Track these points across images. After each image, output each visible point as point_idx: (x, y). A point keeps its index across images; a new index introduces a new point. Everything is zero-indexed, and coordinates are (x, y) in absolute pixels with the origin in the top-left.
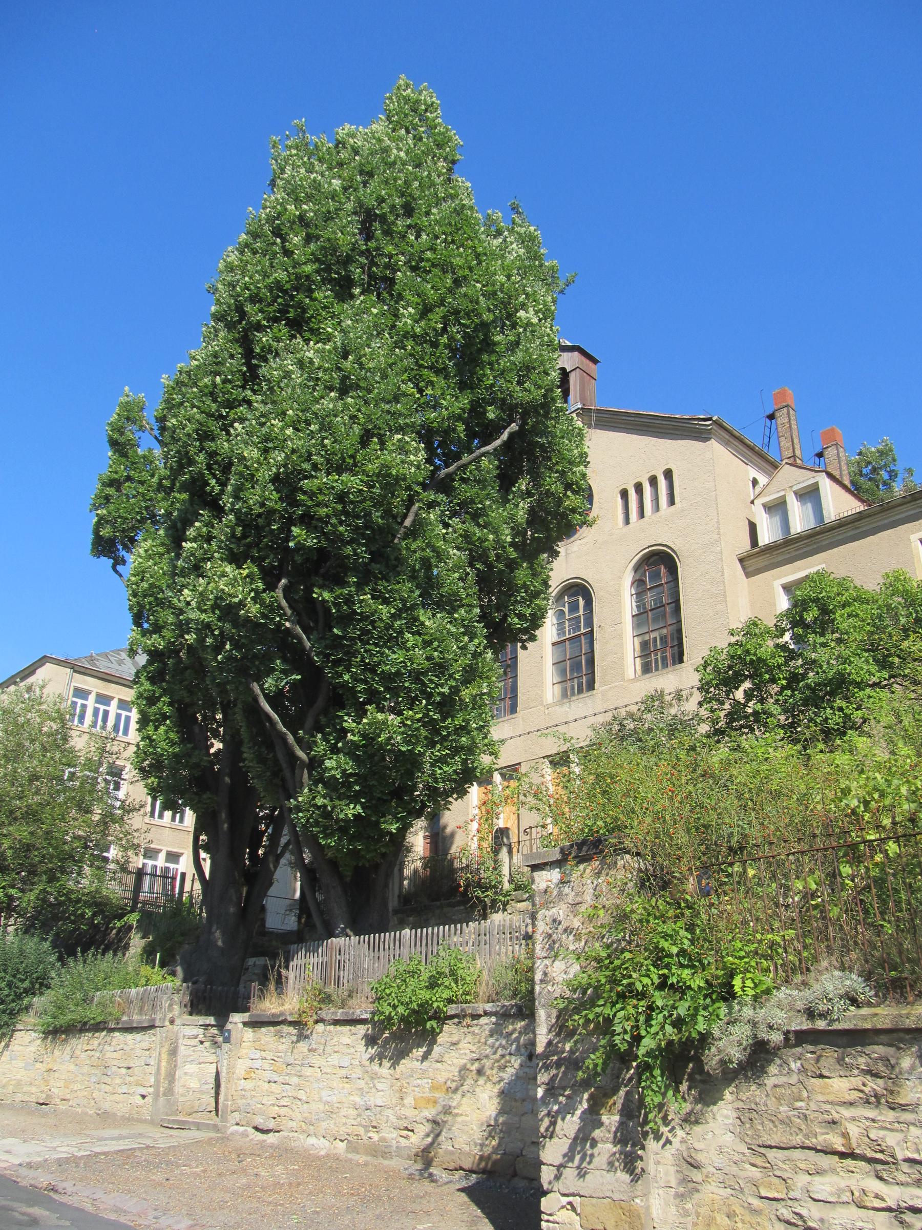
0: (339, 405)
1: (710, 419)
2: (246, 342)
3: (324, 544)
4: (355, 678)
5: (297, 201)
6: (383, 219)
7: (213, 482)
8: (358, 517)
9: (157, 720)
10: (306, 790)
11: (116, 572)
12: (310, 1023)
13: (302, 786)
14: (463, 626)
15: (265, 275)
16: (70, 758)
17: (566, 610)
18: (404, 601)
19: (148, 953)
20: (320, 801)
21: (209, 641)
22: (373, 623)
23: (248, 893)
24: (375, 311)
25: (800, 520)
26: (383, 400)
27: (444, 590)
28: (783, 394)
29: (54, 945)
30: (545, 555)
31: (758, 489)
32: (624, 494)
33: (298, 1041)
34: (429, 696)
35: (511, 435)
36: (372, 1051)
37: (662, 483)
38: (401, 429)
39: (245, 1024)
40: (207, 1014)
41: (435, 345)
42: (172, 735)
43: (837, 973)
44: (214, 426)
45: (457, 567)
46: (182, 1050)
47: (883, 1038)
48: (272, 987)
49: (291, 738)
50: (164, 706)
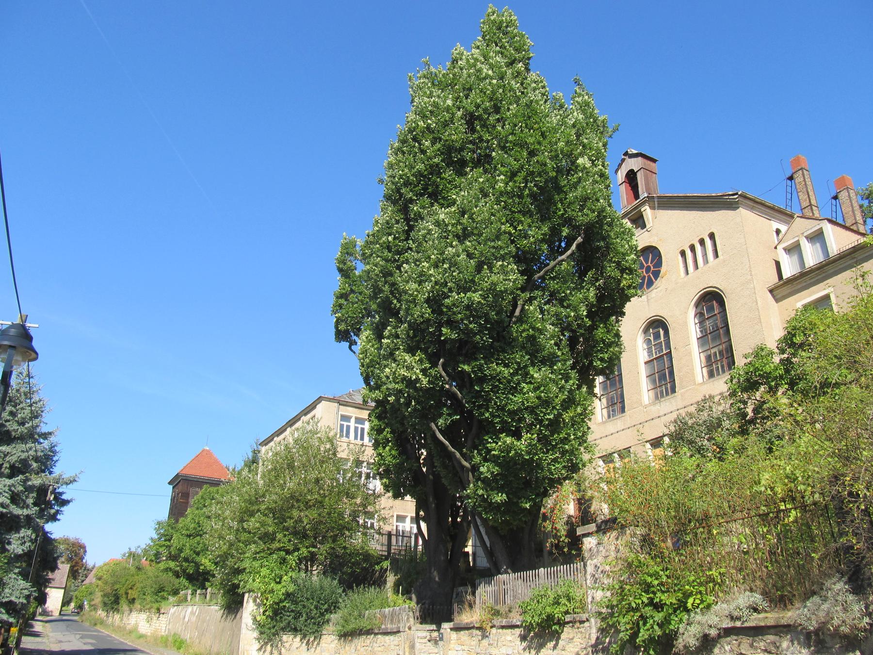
0: (463, 251)
1: (736, 194)
2: (405, 210)
3: (462, 336)
4: (491, 414)
5: (424, 117)
6: (479, 118)
7: (395, 301)
8: (481, 318)
9: (384, 443)
10: (472, 485)
11: (352, 350)
12: (488, 628)
13: (469, 483)
14: (561, 374)
15: (412, 167)
16: (339, 463)
17: (652, 338)
18: (518, 364)
19: (397, 585)
20: (480, 492)
21: (402, 400)
22: (499, 380)
23: (453, 546)
24: (481, 180)
25: (812, 256)
26: (489, 240)
27: (545, 353)
28: (797, 161)
29: (340, 582)
30: (614, 317)
31: (781, 236)
32: (683, 253)
33: (482, 639)
34: (541, 422)
35: (578, 246)
36: (524, 644)
37: (708, 243)
38: (503, 258)
39: (451, 629)
40: (431, 624)
41: (521, 197)
42: (393, 452)
43: (747, 593)
44: (391, 267)
45: (552, 337)
46: (417, 645)
47: (772, 631)
48: (466, 606)
49: (458, 455)
50: (387, 433)
